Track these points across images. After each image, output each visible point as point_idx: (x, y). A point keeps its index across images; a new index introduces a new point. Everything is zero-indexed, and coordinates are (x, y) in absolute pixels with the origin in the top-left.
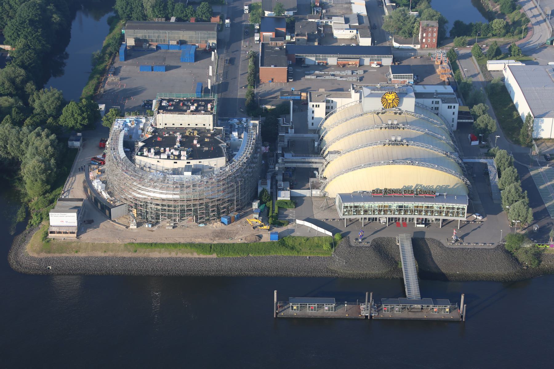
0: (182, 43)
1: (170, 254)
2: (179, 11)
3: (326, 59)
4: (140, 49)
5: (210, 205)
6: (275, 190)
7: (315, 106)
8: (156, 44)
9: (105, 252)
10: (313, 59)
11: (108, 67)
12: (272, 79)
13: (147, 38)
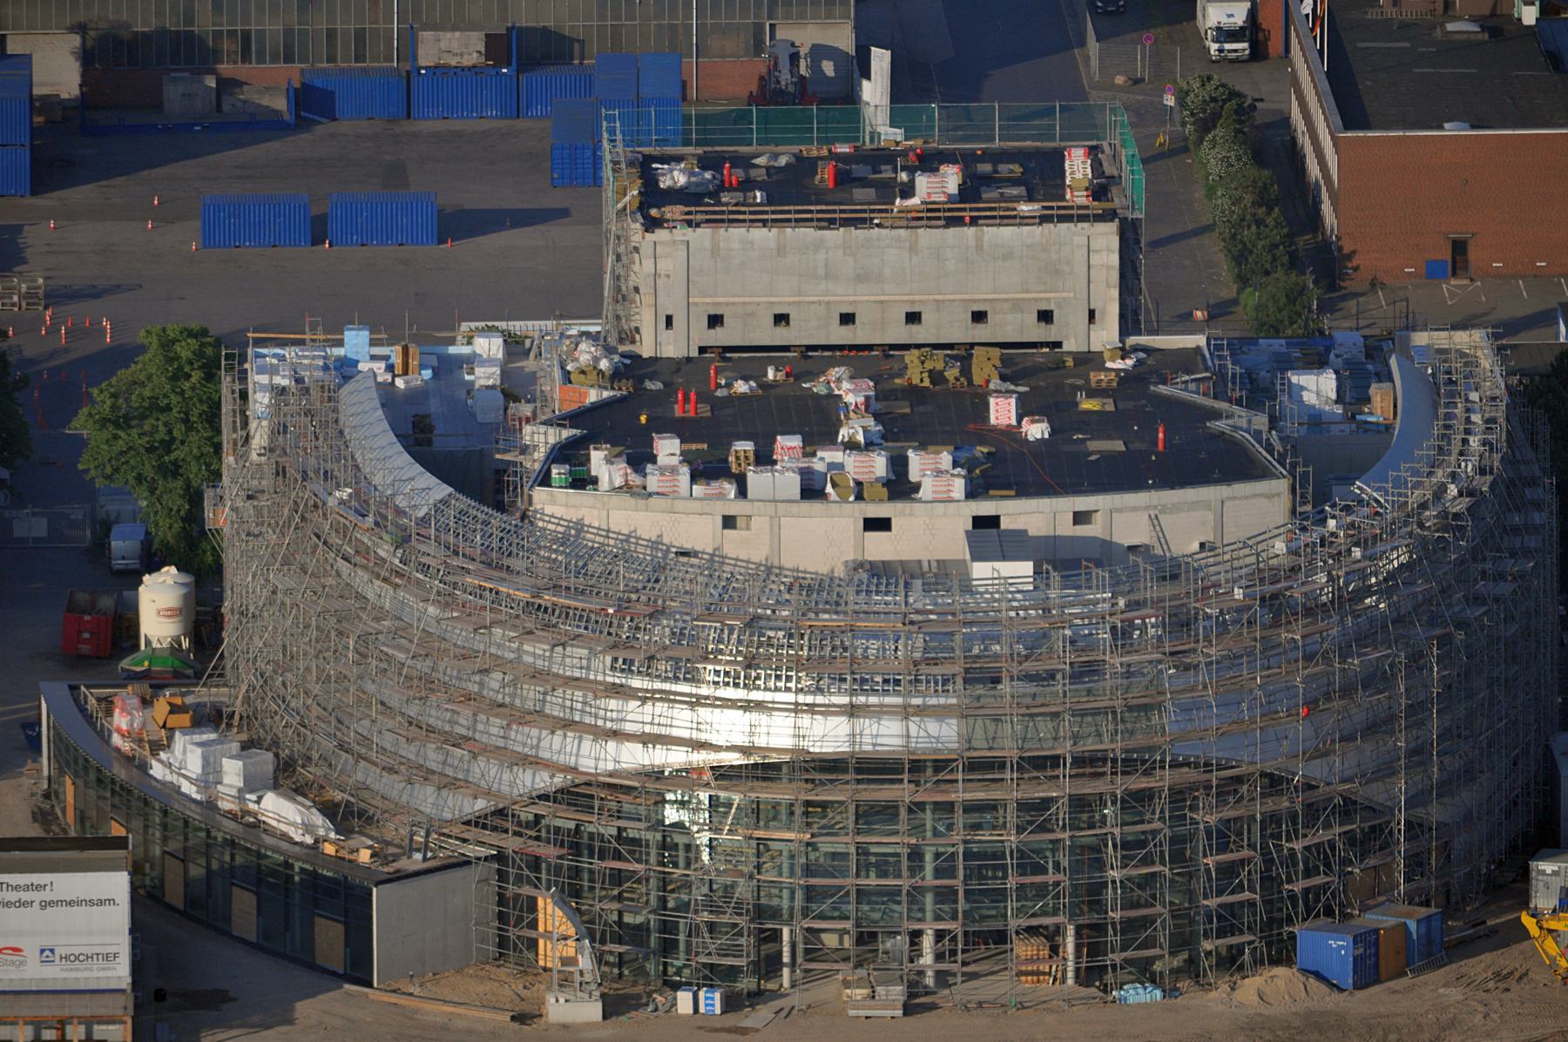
5: (1208, 817)
8: (293, 73)
12: (1459, 248)
13: (205, 23)
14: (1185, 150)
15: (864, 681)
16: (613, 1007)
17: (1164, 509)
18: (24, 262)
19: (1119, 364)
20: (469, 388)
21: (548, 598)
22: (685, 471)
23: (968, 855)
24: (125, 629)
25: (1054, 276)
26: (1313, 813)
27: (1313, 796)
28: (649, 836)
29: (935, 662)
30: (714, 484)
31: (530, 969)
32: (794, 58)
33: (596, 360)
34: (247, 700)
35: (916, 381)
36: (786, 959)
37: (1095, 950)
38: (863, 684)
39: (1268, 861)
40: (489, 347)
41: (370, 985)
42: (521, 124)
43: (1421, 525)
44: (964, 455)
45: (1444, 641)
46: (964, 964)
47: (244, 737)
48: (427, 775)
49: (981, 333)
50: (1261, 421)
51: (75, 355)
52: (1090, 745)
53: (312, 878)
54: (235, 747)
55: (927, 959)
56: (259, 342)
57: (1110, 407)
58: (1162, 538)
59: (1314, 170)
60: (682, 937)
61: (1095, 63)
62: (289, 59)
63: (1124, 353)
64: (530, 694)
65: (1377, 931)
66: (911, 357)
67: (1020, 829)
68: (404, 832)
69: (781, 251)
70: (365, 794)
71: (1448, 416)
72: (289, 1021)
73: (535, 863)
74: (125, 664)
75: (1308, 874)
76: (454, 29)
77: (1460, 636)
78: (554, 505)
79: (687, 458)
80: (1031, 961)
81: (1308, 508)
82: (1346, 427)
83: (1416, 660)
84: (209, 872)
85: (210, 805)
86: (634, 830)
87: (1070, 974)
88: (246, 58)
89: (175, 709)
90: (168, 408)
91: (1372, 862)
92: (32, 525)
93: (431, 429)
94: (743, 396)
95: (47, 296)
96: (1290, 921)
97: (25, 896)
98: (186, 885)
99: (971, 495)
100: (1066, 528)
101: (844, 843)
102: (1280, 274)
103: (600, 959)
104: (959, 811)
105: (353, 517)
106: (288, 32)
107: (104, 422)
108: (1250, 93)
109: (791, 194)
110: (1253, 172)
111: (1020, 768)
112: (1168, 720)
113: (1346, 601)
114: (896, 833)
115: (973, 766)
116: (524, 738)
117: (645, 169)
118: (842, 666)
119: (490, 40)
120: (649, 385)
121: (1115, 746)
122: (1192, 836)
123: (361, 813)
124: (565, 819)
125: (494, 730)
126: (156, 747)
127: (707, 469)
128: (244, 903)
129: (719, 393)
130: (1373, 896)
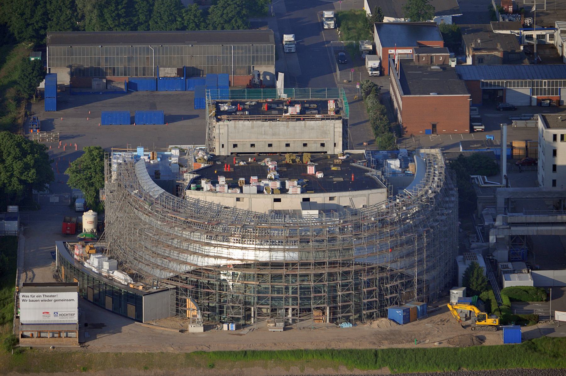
0: (188, 74)
1: (288, 369)
2: (165, 18)
3: (558, 92)
5: (364, 278)
7: (559, 138)
8: (126, 79)
9: (146, 368)
10: (526, 91)
11: (20, 121)
12: (434, 126)
13: (103, 65)
14: (362, 100)
15: (273, 242)
19: (342, 158)
21: (189, 220)
22: (226, 186)
23: (301, 288)
24: (78, 227)
25: (325, 134)
26: (392, 277)
27: (392, 273)
28: (216, 283)
30: (234, 189)
32: (259, 75)
33: (204, 156)
34: (110, 246)
35: (288, 162)
36: (252, 316)
37: (334, 313)
38: (273, 243)
39: (380, 290)
42: (187, 92)
43: (421, 201)
44: (300, 182)
45: (427, 232)
46: (300, 317)
47: (109, 256)
48: (158, 266)
49: (306, 149)
50: (379, 173)
52: (333, 259)
53: (127, 294)
54: (107, 258)
56: (114, 151)
60: (225, 310)
61: (338, 76)
62: (125, 75)
63: (343, 155)
64: (185, 245)
65: (409, 309)
66: (287, 156)
67: (315, 281)
68: (151, 281)
69: (253, 127)
70: (141, 271)
71: (429, 172)
72: (120, 332)
73: (186, 290)
74: (79, 236)
75: (391, 293)
76: (169, 67)
77: (432, 230)
78: (192, 195)
79: (227, 182)
81: (392, 196)
83: (420, 236)
85: (100, 274)
87: (328, 320)
89: (91, 248)
90: (91, 168)
91: (408, 290)
93: (159, 174)
94: (242, 166)
95: (60, 138)
96: (386, 306)
97: (50, 298)
98: (93, 295)
99: (302, 192)
100: (327, 201)
101: (268, 285)
102: (386, 133)
103: (203, 316)
105: (138, 198)
106: (125, 68)
107: (73, 172)
108: (379, 85)
109: (256, 112)
110: (380, 106)
111: (315, 265)
112: (354, 252)
113: (402, 221)
114: (282, 282)
115: (302, 264)
116: (183, 257)
120: (217, 163)
121: (340, 260)
122: (360, 283)
123: (140, 277)
124: (194, 278)
125: (175, 255)
126: (86, 259)
127: (232, 185)
128: (109, 300)
130: (408, 299)
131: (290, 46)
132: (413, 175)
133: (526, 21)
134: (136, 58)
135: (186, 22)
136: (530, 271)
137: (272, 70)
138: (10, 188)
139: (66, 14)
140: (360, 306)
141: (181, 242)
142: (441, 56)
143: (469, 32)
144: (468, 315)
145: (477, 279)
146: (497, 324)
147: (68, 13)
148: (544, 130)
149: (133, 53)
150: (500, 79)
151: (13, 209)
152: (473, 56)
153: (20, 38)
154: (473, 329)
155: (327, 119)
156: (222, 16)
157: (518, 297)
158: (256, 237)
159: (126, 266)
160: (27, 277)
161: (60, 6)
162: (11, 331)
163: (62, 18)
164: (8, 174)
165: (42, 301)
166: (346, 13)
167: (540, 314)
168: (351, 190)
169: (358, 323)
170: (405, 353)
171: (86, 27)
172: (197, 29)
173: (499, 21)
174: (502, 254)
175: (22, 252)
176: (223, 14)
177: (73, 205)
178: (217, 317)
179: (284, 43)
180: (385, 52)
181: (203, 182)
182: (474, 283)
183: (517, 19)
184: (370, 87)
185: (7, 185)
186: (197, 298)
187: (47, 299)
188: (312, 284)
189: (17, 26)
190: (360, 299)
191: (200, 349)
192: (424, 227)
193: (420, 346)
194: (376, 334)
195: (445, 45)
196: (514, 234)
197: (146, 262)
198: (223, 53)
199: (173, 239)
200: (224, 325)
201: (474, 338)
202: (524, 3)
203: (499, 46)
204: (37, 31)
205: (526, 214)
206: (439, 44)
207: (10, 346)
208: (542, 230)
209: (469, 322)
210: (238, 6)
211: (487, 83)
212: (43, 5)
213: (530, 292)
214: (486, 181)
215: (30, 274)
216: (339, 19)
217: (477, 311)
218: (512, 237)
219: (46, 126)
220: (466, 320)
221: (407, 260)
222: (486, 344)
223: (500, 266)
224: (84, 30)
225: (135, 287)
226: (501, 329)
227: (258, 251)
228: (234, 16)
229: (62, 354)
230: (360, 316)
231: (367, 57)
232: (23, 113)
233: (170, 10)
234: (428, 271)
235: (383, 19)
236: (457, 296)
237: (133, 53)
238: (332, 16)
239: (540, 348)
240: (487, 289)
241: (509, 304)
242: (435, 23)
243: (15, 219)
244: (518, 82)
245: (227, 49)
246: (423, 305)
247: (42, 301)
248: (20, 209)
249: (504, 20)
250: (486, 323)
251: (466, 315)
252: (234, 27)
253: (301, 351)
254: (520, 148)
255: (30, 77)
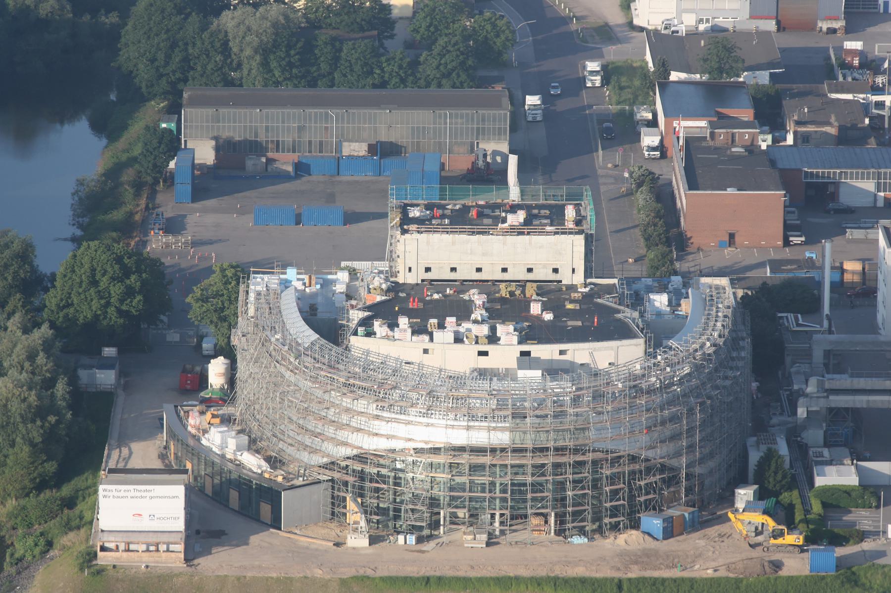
0: (384, 151)
2: (357, 68)
4: (236, 170)
5: (607, 472)
6: (805, 465)
8: (295, 157)
10: (869, 185)
11: (137, 217)
12: (732, 236)
13: (262, 138)
14: (632, 194)
15: (473, 416)
16: (373, 540)
17: (595, 350)
18: (185, 229)
19: (583, 290)
20: (334, 293)
21: (352, 381)
22: (410, 331)
23: (513, 485)
24: (202, 381)
25: (557, 256)
26: (649, 470)
27: (648, 464)
28: (389, 474)
29: (500, 410)
30: (421, 336)
31: (343, 524)
32: (485, 156)
33: (381, 284)
34: (241, 414)
35: (504, 295)
36: (442, 523)
37: (562, 522)
38: (473, 418)
39: (631, 489)
40: (343, 277)
41: (280, 529)
42: (381, 178)
43: (694, 358)
44: (519, 326)
45: (702, 404)
46: (511, 525)
47: (239, 428)
48: (306, 447)
49: (530, 277)
50: (636, 314)
51: (201, 267)
52: (561, 443)
53: (260, 487)
54: (233, 433)
55: (497, 524)
56: (255, 273)
57: (578, 308)
58: (594, 360)
59: (679, 204)
60: (402, 514)
61: (601, 159)
62: (294, 151)
63: (586, 285)
64: (345, 418)
65: (672, 517)
66: (502, 286)
67: (533, 475)
68: (296, 469)
69: (453, 243)
70: (282, 454)
71: (709, 314)
72: (247, 544)
73: (346, 484)
74: (202, 394)
75: (647, 493)
76: (356, 141)
77: (709, 402)
78: (358, 343)
79: (411, 326)
80: (537, 525)
81: (652, 350)
82: (670, 316)
83: (691, 412)
84: (221, 482)
85: (223, 456)
86: (384, 471)
87: (553, 531)
88: (277, 151)
89: (214, 416)
90: (223, 295)
91: (672, 489)
92: (173, 336)
93: (316, 309)
94: (436, 300)
95: (192, 243)
96: (639, 513)
97: (144, 494)
98: (213, 487)
99: (520, 343)
100: (557, 356)
101: (464, 479)
102: (660, 246)
103: (369, 521)
104: (509, 467)
105: (281, 346)
106: (294, 141)
107: (197, 300)
108: (657, 172)
109: (460, 221)
110: (654, 205)
111: (533, 452)
112: (592, 434)
113: (665, 387)
114: (484, 475)
115: (515, 451)
116: (342, 435)
117: (404, 209)
118: (465, 410)
119: (370, 146)
120: (401, 295)
121: (570, 444)
122: (601, 479)
123: (280, 461)
124: (358, 467)
125: (331, 431)
126: (205, 432)
127: (417, 330)
128: (234, 495)
129: (428, 298)
130: (672, 502)
131: (534, 112)
132: (687, 317)
133: (877, 80)
134: (310, 127)
135: (387, 75)
136: (855, 462)
137: (504, 147)
138: (105, 323)
139: (216, 61)
140: (601, 512)
141: (339, 413)
142: (746, 134)
143: (793, 96)
144: (760, 528)
145: (776, 473)
146: (801, 543)
147: (218, 59)
148: (887, 250)
149: (305, 119)
150: (831, 168)
151: (109, 351)
152: (795, 133)
153: (149, 93)
154: (766, 549)
155: (563, 233)
156: (438, 68)
157: (836, 501)
158: (449, 410)
159: (260, 444)
160: (120, 456)
161: (207, 50)
162: (87, 540)
163: (209, 67)
164: (103, 302)
165: (132, 497)
166: (620, 64)
167: (867, 528)
168: (591, 341)
169: (597, 536)
170: (663, 584)
171: (244, 81)
172: (402, 86)
173: (837, 79)
174: (814, 436)
175: (119, 415)
176: (440, 64)
177: (199, 346)
178: (390, 524)
179: (527, 108)
180: (668, 124)
181: (377, 324)
182: (771, 480)
183: (868, 76)
184: (643, 175)
185: (101, 318)
186: (362, 496)
187: (139, 494)
188: (529, 479)
189: (146, 76)
190: (600, 501)
191: (361, 572)
192: (697, 397)
193: (686, 574)
194: (622, 554)
195: (757, 116)
196: (833, 405)
197: (290, 441)
198: (434, 123)
199: (328, 408)
200: (399, 536)
201: (766, 564)
202: (876, 53)
203: (833, 119)
204: (173, 84)
205: (852, 376)
206: (747, 114)
207: (84, 562)
208: (875, 401)
209: (760, 539)
210: (462, 53)
211: (812, 173)
212: (182, 47)
213: (854, 494)
214: (801, 322)
215: (125, 451)
216: (608, 73)
217: (771, 523)
218: (830, 410)
219: (173, 226)
220: (756, 535)
221: (672, 445)
222: (784, 573)
223: (811, 453)
224: (241, 85)
225: (272, 477)
226: (807, 551)
227: (451, 430)
228: (456, 68)
229: (159, 577)
230: (600, 527)
231: (644, 130)
232: (143, 206)
233: (364, 57)
234: (701, 461)
235: (669, 74)
236: (745, 498)
237: (305, 119)
238: (598, 69)
239: (863, 580)
240: (790, 489)
241: (821, 511)
242: (744, 83)
243: (111, 367)
244: (857, 173)
245: (440, 117)
246: (693, 512)
247: (132, 497)
248: (119, 352)
249: (844, 79)
250: (784, 542)
251: (756, 528)
252: (455, 83)
253: (510, 578)
254: (853, 273)
255: (156, 153)
